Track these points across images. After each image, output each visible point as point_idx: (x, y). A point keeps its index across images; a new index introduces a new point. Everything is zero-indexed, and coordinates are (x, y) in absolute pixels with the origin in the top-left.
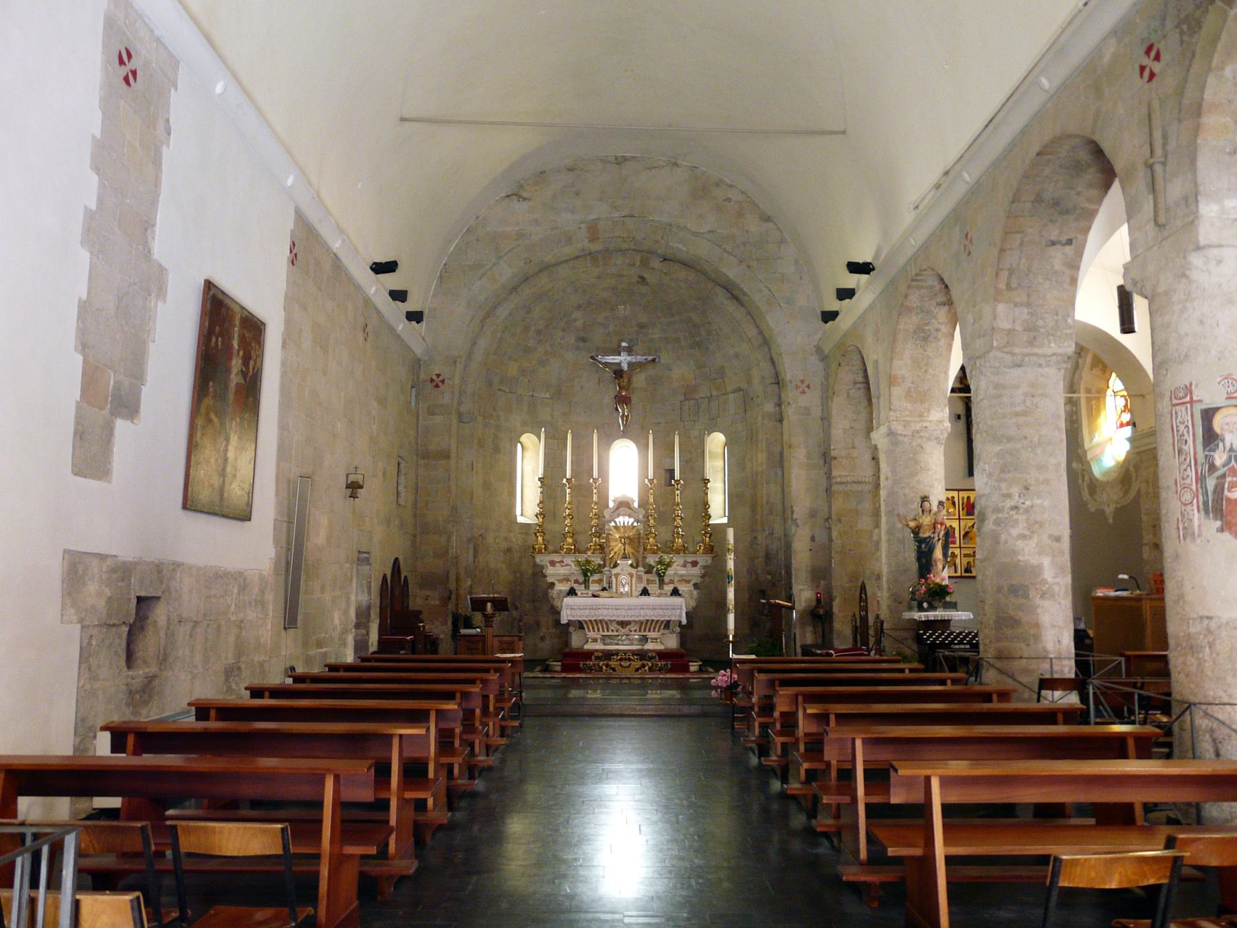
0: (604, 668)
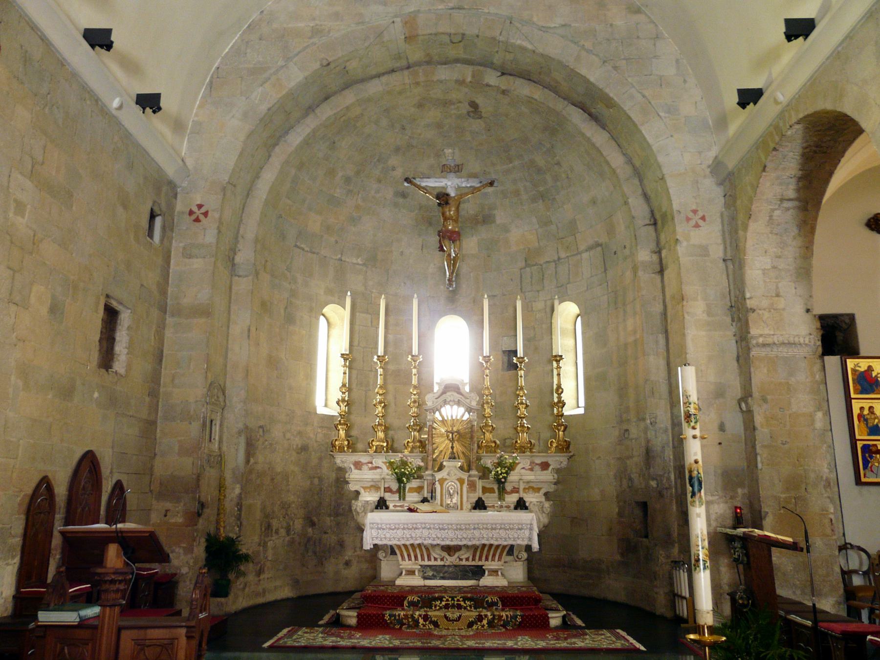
0: (421, 621)
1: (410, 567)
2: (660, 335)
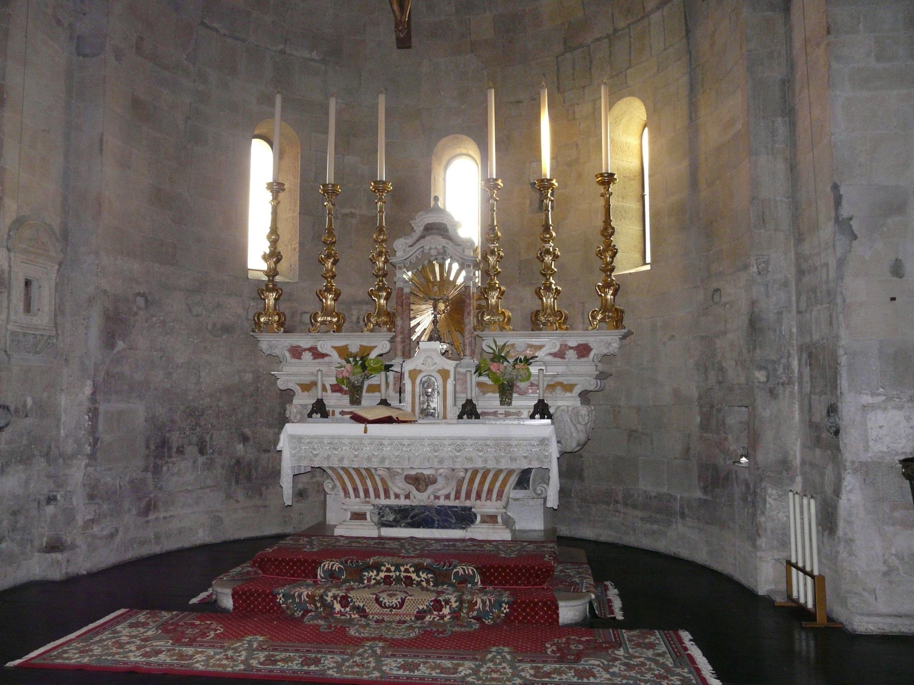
0: (337, 607)
1: (357, 507)
2: (779, 119)
